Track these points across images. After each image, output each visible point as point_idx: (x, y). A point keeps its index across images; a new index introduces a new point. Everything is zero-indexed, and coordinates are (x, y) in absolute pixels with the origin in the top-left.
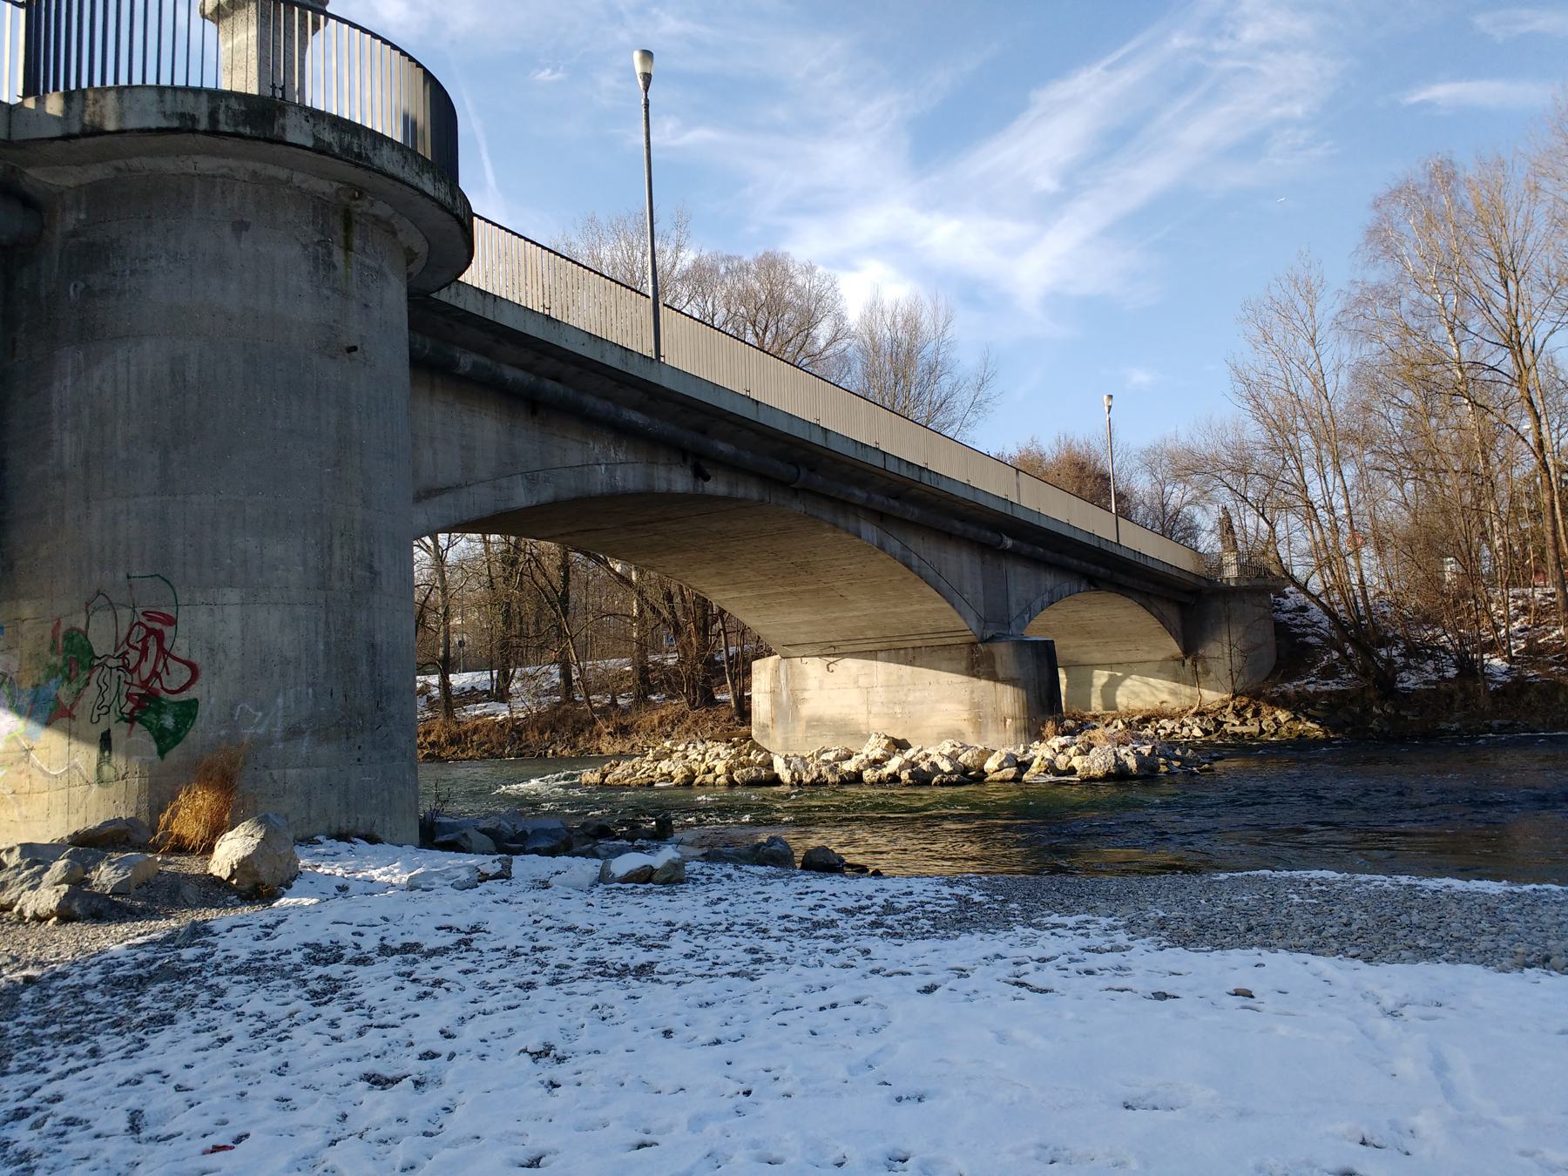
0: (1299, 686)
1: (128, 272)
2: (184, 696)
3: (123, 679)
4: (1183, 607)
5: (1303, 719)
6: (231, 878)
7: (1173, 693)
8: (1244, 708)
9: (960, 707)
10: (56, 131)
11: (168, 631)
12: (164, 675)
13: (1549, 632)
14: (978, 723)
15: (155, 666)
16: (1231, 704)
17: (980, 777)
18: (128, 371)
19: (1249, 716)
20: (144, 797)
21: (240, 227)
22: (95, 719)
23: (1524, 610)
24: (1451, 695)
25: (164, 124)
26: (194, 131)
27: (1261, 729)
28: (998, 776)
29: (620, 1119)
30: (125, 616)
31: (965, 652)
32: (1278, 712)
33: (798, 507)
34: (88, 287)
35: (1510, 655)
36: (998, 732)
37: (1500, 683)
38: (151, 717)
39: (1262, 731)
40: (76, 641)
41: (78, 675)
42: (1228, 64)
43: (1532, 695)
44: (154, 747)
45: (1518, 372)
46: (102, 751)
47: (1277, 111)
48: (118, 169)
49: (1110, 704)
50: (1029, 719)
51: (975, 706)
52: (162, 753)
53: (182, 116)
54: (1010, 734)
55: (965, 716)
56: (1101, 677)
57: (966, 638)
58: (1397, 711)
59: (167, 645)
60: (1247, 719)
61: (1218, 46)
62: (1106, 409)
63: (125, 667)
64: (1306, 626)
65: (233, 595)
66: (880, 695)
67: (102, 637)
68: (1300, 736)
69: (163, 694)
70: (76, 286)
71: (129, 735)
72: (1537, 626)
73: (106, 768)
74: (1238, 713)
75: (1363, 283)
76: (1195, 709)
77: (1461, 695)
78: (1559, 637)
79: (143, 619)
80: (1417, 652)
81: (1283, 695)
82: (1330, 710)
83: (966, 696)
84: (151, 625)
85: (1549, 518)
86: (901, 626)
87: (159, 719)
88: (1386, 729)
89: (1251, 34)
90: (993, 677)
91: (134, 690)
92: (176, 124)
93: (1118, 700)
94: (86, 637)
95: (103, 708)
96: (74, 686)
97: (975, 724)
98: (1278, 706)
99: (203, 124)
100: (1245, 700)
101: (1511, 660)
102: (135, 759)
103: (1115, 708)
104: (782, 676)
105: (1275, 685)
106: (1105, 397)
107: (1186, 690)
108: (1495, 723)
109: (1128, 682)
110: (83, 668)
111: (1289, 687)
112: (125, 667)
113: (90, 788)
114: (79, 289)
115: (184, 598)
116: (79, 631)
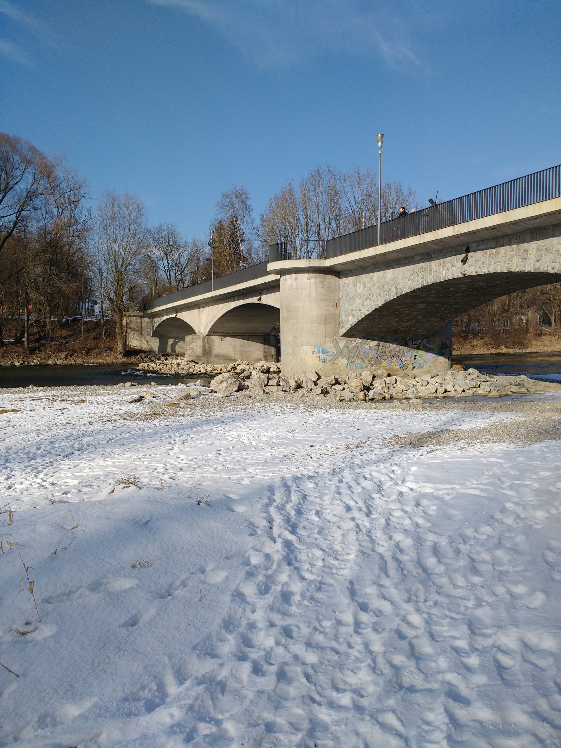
29: (241, 582)
49: (173, 350)
56: (171, 341)
66: (238, 348)
83: (262, 349)
90: (270, 345)
93: (176, 349)
103: (175, 352)
104: (206, 341)
109: (180, 343)
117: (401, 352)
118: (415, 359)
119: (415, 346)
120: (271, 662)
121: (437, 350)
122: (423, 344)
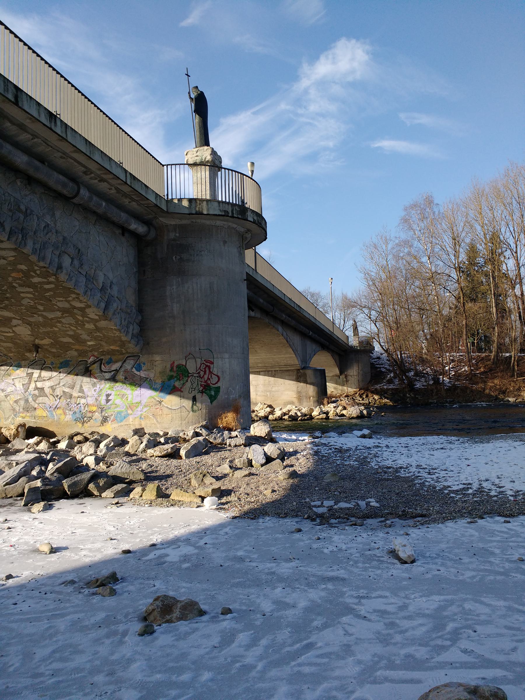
0: (380, 386)
1: (195, 255)
2: (216, 386)
3: (199, 380)
4: (340, 355)
5: (384, 398)
6: (265, 436)
7: (335, 388)
8: (363, 394)
9: (293, 393)
10: (187, 212)
11: (212, 366)
12: (211, 379)
13: (461, 369)
14: (300, 398)
15: (208, 376)
16: (358, 392)
17: (311, 418)
18: (197, 286)
19: (364, 397)
20: (207, 415)
21: (225, 242)
22: (190, 392)
23: (453, 361)
24: (432, 390)
25: (220, 213)
26: (228, 216)
27: (369, 402)
28: (318, 417)
30: (199, 361)
31: (295, 373)
32: (374, 396)
33: (267, 320)
34: (181, 258)
35: (449, 377)
36: (307, 402)
37: (448, 386)
38: (208, 392)
39: (370, 403)
40: (181, 368)
41: (183, 378)
42: (303, 120)
43: (459, 391)
44: (209, 401)
45: (457, 278)
46: (193, 402)
47: (323, 143)
48: (192, 222)
50: (318, 397)
51: (299, 393)
52: (211, 402)
53: (225, 211)
54: (312, 403)
55: (295, 396)
57: (296, 368)
58: (415, 396)
59: (211, 370)
60: (364, 398)
61: (300, 111)
62: (330, 283)
63: (200, 376)
64: (380, 365)
65: (227, 356)
67: (191, 367)
68: (385, 404)
69: (211, 385)
70: (176, 257)
71: (202, 397)
72: (457, 366)
73: (195, 407)
74: (361, 396)
75: (399, 238)
76: (345, 394)
77: (436, 391)
78: (465, 370)
79: (204, 362)
80: (418, 374)
81: (376, 389)
82: (393, 395)
83: (295, 388)
84: (206, 364)
85: (465, 329)
86: (273, 363)
87: (210, 392)
88: (412, 402)
89: (313, 108)
90: (306, 382)
91: (203, 383)
92: (223, 214)
94: (186, 367)
95: (193, 389)
96: (182, 382)
97: (299, 399)
98: (374, 394)
99: (230, 215)
100: (363, 391)
101: (450, 378)
102: (204, 404)
105: (372, 386)
106: (330, 279)
107: (340, 387)
108: (448, 400)
110: (185, 376)
111: (378, 387)
112: (200, 376)
113: (189, 413)
114: (177, 258)
115: (215, 356)
116: (183, 365)
117: (77, 387)
118: (108, 401)
119: (108, 376)
120: (403, 629)
121: (159, 381)
122: (126, 371)
